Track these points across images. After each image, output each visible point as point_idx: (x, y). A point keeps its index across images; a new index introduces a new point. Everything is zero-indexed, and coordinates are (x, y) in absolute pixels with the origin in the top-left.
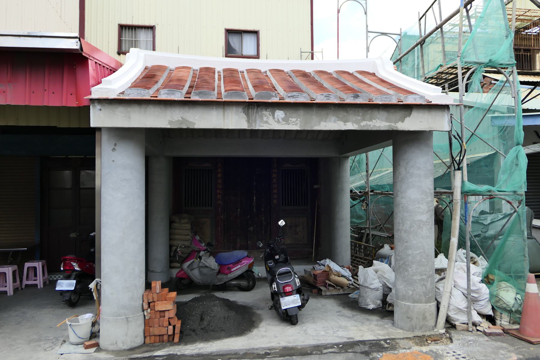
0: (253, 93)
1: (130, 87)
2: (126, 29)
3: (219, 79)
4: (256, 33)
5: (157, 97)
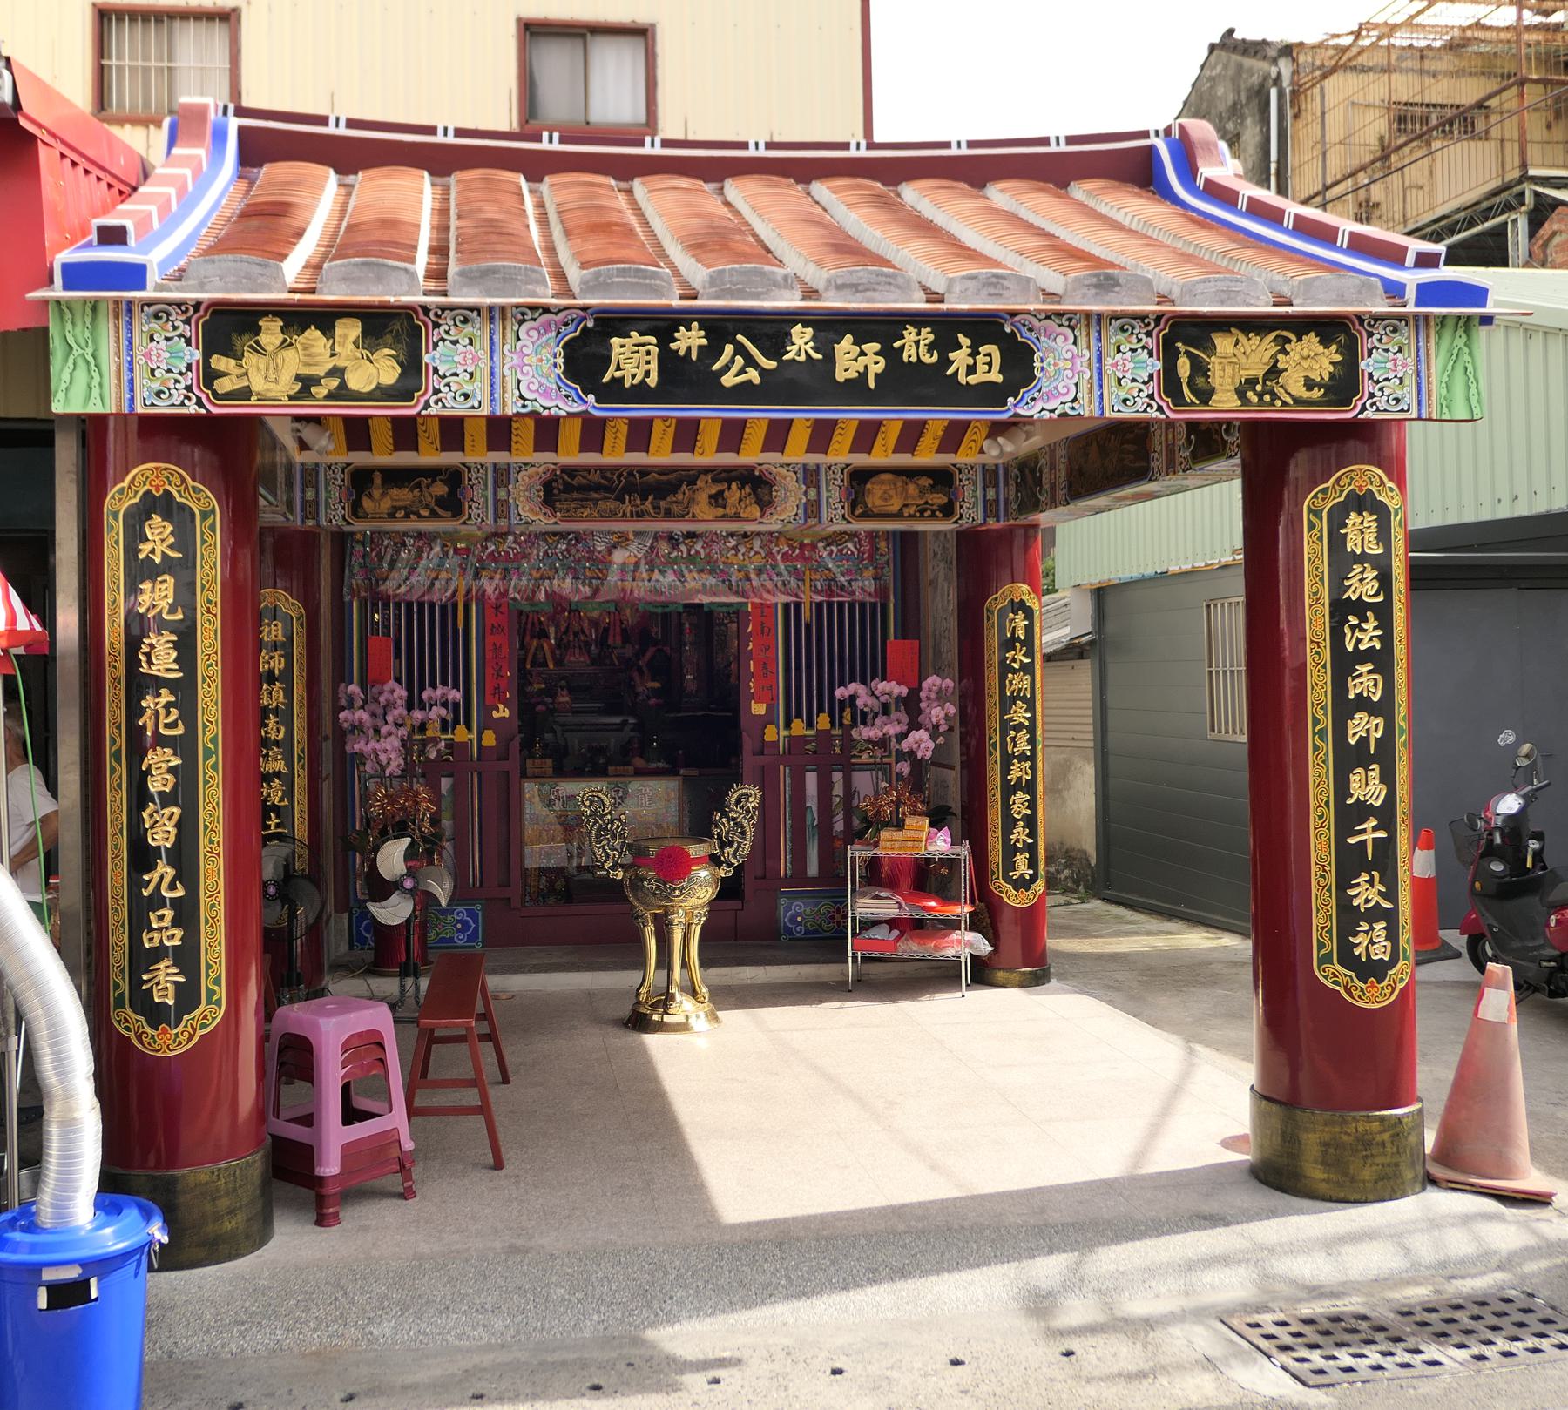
0: (696, 272)
1: (211, 251)
2: (120, 19)
3: (543, 220)
4: (641, 33)
5: (313, 291)
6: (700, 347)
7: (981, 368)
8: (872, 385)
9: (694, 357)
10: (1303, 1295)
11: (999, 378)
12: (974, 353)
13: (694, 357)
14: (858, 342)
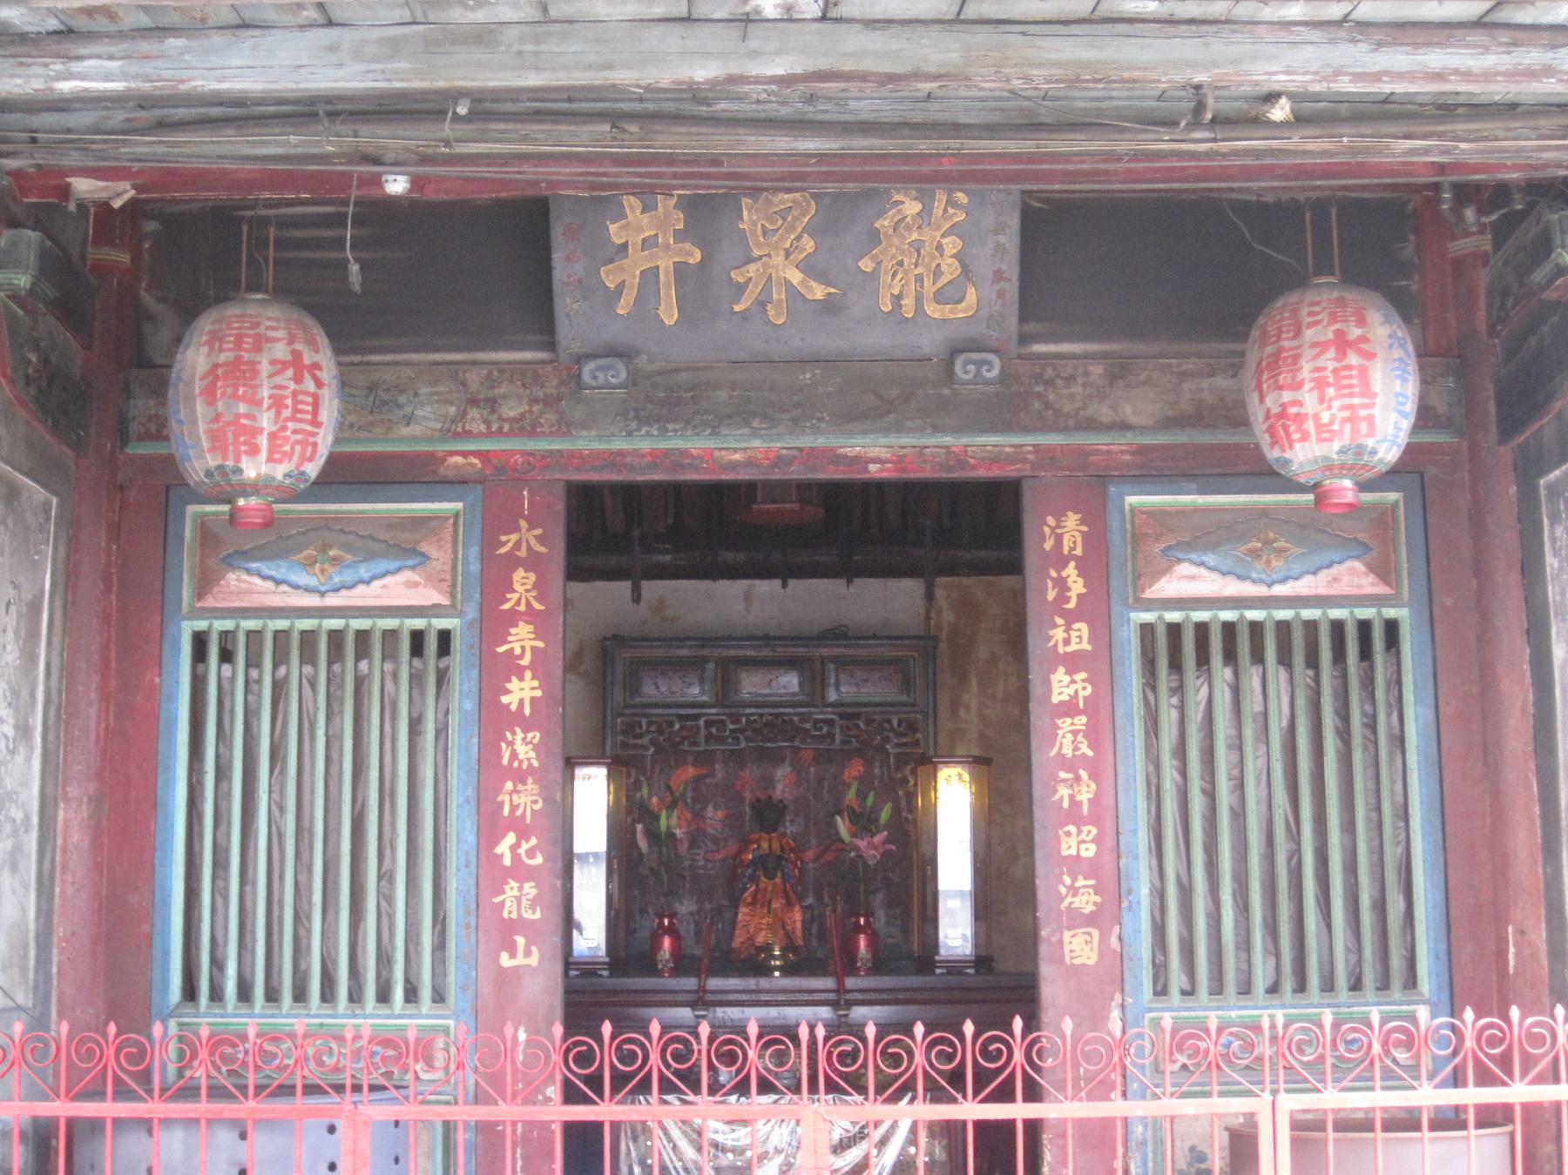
6: (533, 699)
7: (1074, 640)
8: (542, 549)
9: (527, 711)
10: (415, 715)
11: (1089, 648)
12: (1068, 629)
13: (527, 711)
14: (1070, 672)
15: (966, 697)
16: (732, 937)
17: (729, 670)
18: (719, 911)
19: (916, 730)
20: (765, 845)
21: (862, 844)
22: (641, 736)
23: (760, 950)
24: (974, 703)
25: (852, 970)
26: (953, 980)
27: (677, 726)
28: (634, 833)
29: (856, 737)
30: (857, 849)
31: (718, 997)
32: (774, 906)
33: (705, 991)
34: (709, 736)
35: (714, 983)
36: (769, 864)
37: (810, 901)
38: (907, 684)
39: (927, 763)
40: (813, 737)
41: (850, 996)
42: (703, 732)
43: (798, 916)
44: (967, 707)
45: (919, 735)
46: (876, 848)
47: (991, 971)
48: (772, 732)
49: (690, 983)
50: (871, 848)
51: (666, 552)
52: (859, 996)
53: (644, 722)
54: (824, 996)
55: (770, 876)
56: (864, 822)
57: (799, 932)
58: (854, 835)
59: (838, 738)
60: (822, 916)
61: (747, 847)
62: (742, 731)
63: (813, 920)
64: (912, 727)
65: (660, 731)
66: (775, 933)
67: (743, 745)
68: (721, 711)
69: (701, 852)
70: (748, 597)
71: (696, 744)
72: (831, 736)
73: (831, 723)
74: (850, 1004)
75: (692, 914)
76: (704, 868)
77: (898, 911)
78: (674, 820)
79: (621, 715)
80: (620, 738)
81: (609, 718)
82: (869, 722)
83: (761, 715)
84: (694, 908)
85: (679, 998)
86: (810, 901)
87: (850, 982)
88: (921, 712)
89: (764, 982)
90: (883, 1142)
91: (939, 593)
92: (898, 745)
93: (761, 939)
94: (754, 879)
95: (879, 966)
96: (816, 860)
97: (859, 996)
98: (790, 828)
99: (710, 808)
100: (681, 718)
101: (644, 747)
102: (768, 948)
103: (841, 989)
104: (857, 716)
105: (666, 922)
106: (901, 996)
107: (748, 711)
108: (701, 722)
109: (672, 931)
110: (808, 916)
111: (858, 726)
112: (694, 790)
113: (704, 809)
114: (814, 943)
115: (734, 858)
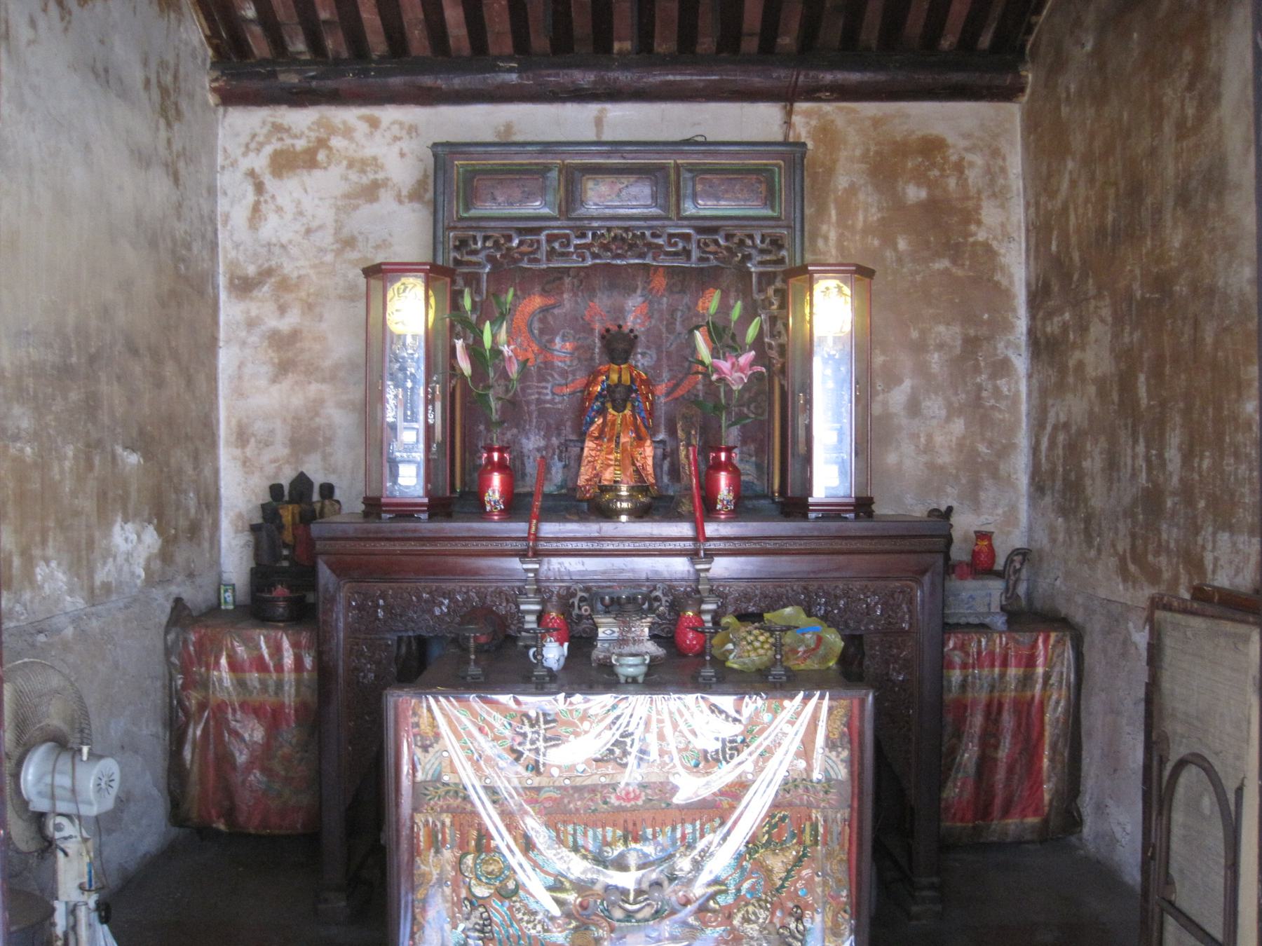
15: (824, 228)
16: (577, 475)
17: (573, 178)
18: (565, 446)
19: (781, 247)
20: (615, 377)
21: (725, 365)
22: (475, 252)
23: (604, 489)
24: (833, 235)
25: (709, 509)
26: (833, 526)
27: (515, 243)
28: (453, 349)
29: (715, 253)
30: (717, 370)
31: (554, 545)
32: (623, 439)
33: (537, 539)
34: (552, 253)
35: (549, 529)
36: (618, 396)
37: (661, 436)
38: (770, 198)
39: (803, 273)
40: (668, 254)
41: (712, 545)
42: (545, 247)
43: (648, 450)
44: (826, 239)
45: (784, 253)
46: (741, 370)
47: (870, 515)
48: (620, 255)
49: (519, 528)
50: (736, 371)
51: (511, 70)
52: (721, 545)
53: (479, 236)
54: (679, 545)
55: (619, 408)
56: (724, 339)
57: (650, 469)
58: (715, 354)
59: (695, 254)
60: (675, 452)
61: (595, 378)
62: (587, 246)
63: (664, 456)
64: (777, 243)
65: (497, 245)
66: (624, 471)
67: (589, 262)
68: (565, 223)
69: (549, 386)
70: (599, 122)
71: (537, 261)
72: (687, 253)
73: (686, 237)
74: (710, 555)
75: (538, 450)
76: (552, 401)
77: (752, 447)
78: (503, 336)
79: (454, 228)
80: (453, 254)
81: (440, 233)
82: (728, 237)
83: (609, 229)
84: (542, 443)
85: (509, 545)
86: (661, 436)
87: (710, 529)
88: (788, 227)
89: (607, 528)
90: (766, 755)
91: (796, 119)
92: (762, 263)
93: (608, 476)
94: (602, 412)
95: (740, 510)
96: (668, 394)
97: (721, 545)
98: (642, 361)
99: (558, 340)
100: (520, 231)
101: (478, 264)
102: (613, 488)
103: (699, 536)
104: (715, 230)
105: (496, 456)
106: (770, 545)
107: (595, 224)
108: (543, 237)
109: (728, 466)
110: (660, 451)
111: (716, 242)
112: (542, 321)
113: (552, 341)
114: (666, 479)
115: (582, 392)
